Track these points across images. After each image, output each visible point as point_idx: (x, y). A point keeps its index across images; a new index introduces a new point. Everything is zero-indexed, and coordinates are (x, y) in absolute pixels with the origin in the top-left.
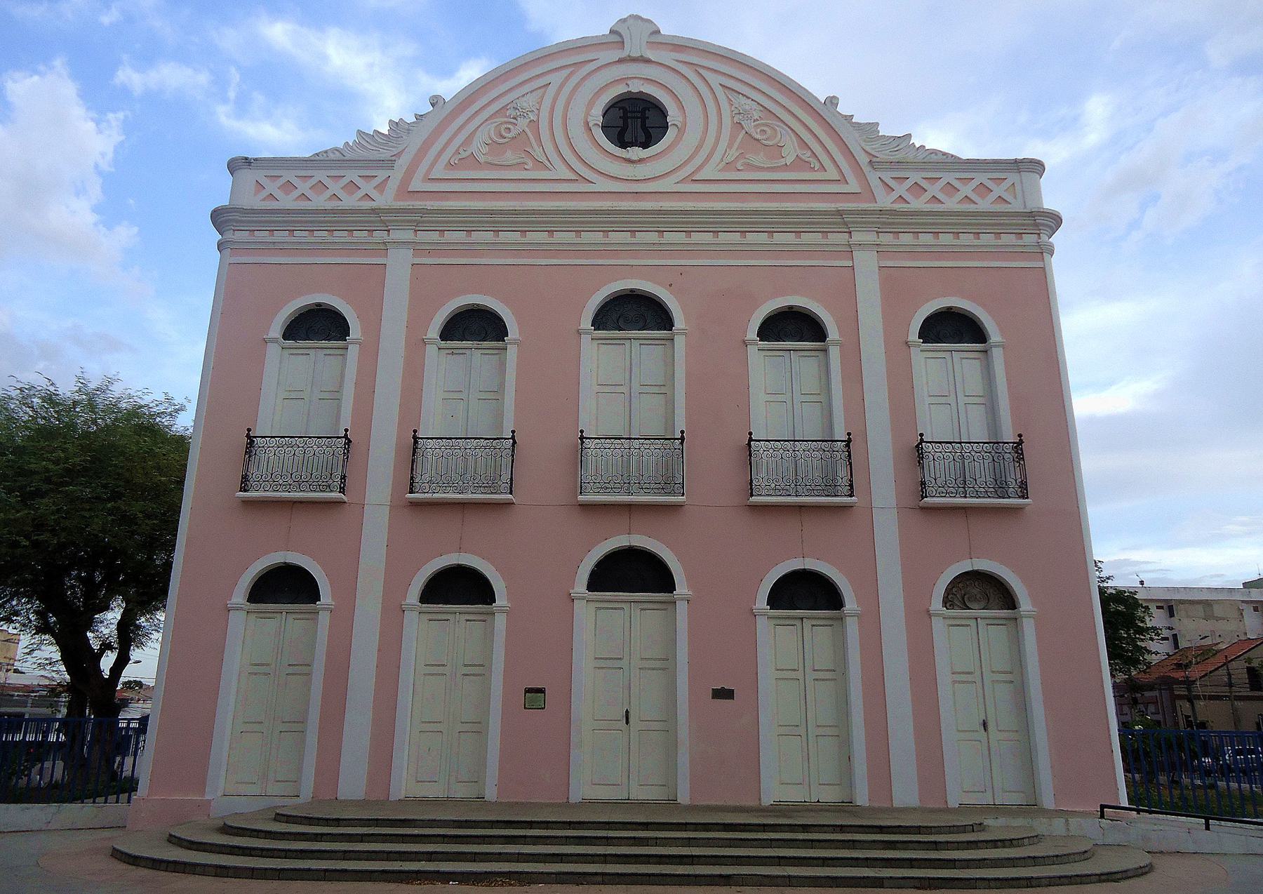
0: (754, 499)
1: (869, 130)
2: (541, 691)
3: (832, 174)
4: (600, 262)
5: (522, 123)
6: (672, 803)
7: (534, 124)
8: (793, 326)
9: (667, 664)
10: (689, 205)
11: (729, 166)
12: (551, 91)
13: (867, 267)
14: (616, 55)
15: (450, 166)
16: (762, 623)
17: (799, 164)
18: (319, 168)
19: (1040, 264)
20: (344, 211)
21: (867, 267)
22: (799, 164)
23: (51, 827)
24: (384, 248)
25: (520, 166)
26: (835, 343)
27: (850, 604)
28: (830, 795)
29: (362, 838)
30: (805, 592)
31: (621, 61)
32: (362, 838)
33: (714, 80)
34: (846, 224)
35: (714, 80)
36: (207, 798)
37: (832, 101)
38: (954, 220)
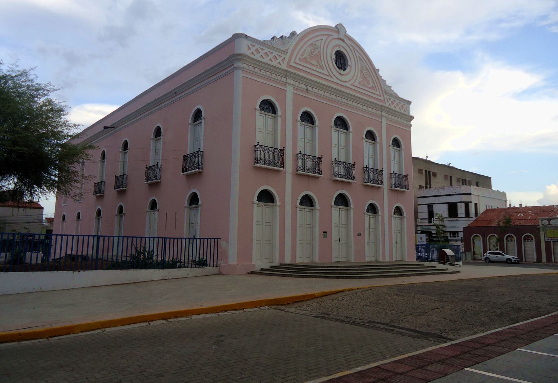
0: (256, 165)
1: (385, 81)
2: (326, 232)
3: (378, 93)
4: (357, 112)
5: (317, 51)
6: (348, 261)
7: (319, 52)
8: (268, 107)
9: (347, 225)
10: (354, 94)
11: (305, 60)
12: (323, 41)
13: (290, 90)
14: (336, 36)
15: (323, 69)
16: (255, 206)
17: (372, 88)
18: (276, 51)
19: (285, 88)
20: (262, 62)
21: (290, 90)
22: (372, 88)
23: (189, 276)
24: (286, 84)
25: (316, 66)
26: (318, 127)
27: (278, 201)
28: (373, 259)
29: (357, 270)
30: (266, 197)
31: (338, 38)
32: (357, 270)
33: (357, 53)
34: (286, 75)
35: (357, 53)
36: (253, 263)
37: (378, 70)
38: (363, 101)
